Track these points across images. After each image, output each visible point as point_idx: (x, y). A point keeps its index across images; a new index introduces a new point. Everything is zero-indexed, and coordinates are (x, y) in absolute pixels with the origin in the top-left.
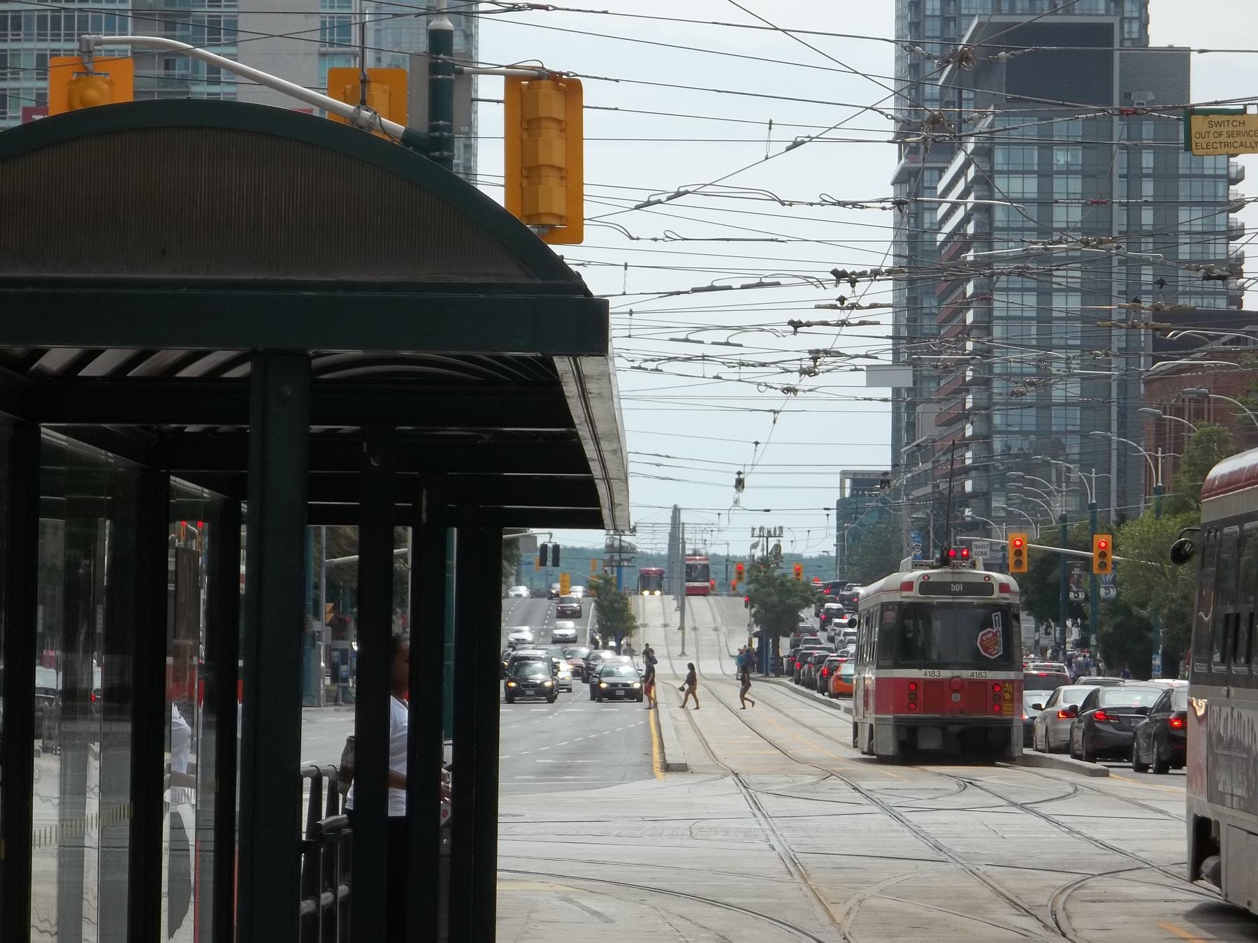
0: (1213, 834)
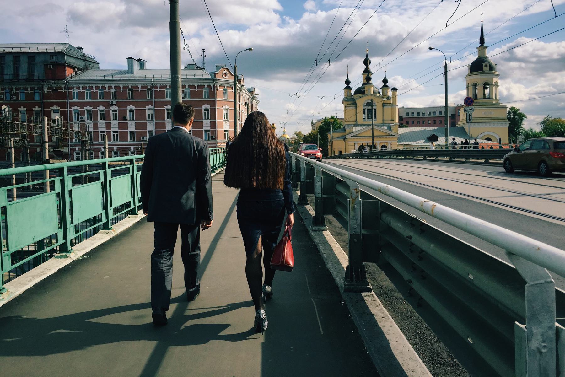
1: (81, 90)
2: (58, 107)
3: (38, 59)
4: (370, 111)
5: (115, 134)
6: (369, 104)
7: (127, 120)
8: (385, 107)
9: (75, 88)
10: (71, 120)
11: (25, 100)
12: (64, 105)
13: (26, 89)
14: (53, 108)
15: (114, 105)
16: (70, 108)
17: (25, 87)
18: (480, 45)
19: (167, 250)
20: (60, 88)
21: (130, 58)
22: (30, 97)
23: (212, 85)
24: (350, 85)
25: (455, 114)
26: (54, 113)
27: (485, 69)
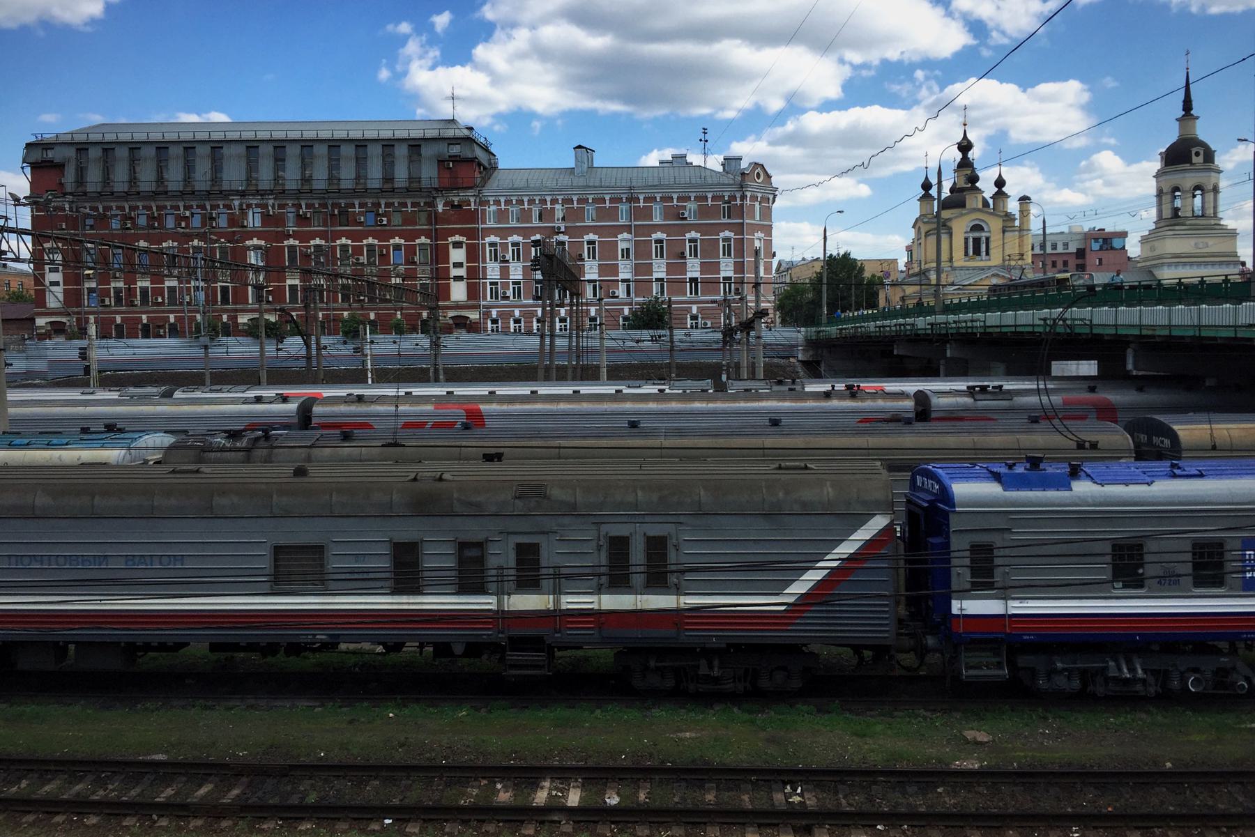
1: (503, 207)
2: (461, 238)
4: (977, 242)
6: (977, 228)
8: (1006, 234)
9: (492, 203)
13: (405, 205)
15: (562, 232)
16: (483, 239)
18: (1184, 113)
21: (580, 147)
22: (208, 219)
23: (738, 195)
25: (1084, 249)
27: (1195, 159)
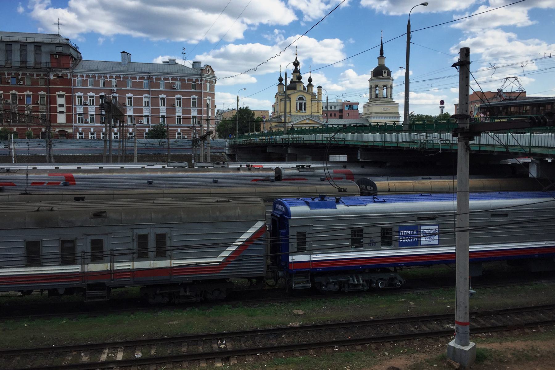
0: (26, 291)
1: (85, 78)
3: (44, 49)
5: (80, 117)
7: (126, 106)
9: (79, 76)
10: (75, 104)
11: (31, 85)
12: (69, 91)
13: (33, 75)
14: (59, 93)
15: (115, 92)
17: (9, 72)
19: (514, 161)
20: (65, 76)
21: (124, 52)
23: (199, 79)
24: (311, 83)
26: (59, 97)
27: (384, 75)
